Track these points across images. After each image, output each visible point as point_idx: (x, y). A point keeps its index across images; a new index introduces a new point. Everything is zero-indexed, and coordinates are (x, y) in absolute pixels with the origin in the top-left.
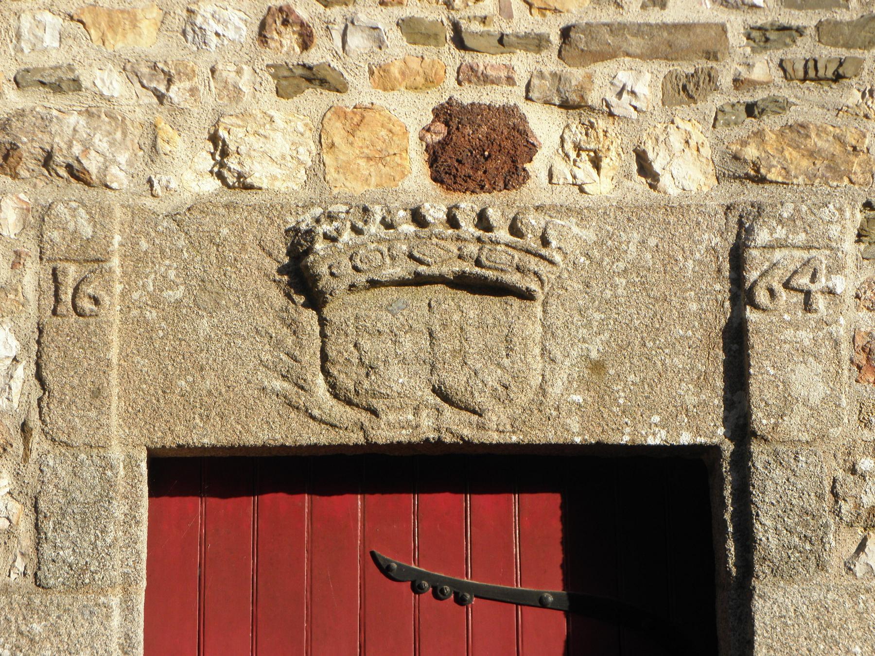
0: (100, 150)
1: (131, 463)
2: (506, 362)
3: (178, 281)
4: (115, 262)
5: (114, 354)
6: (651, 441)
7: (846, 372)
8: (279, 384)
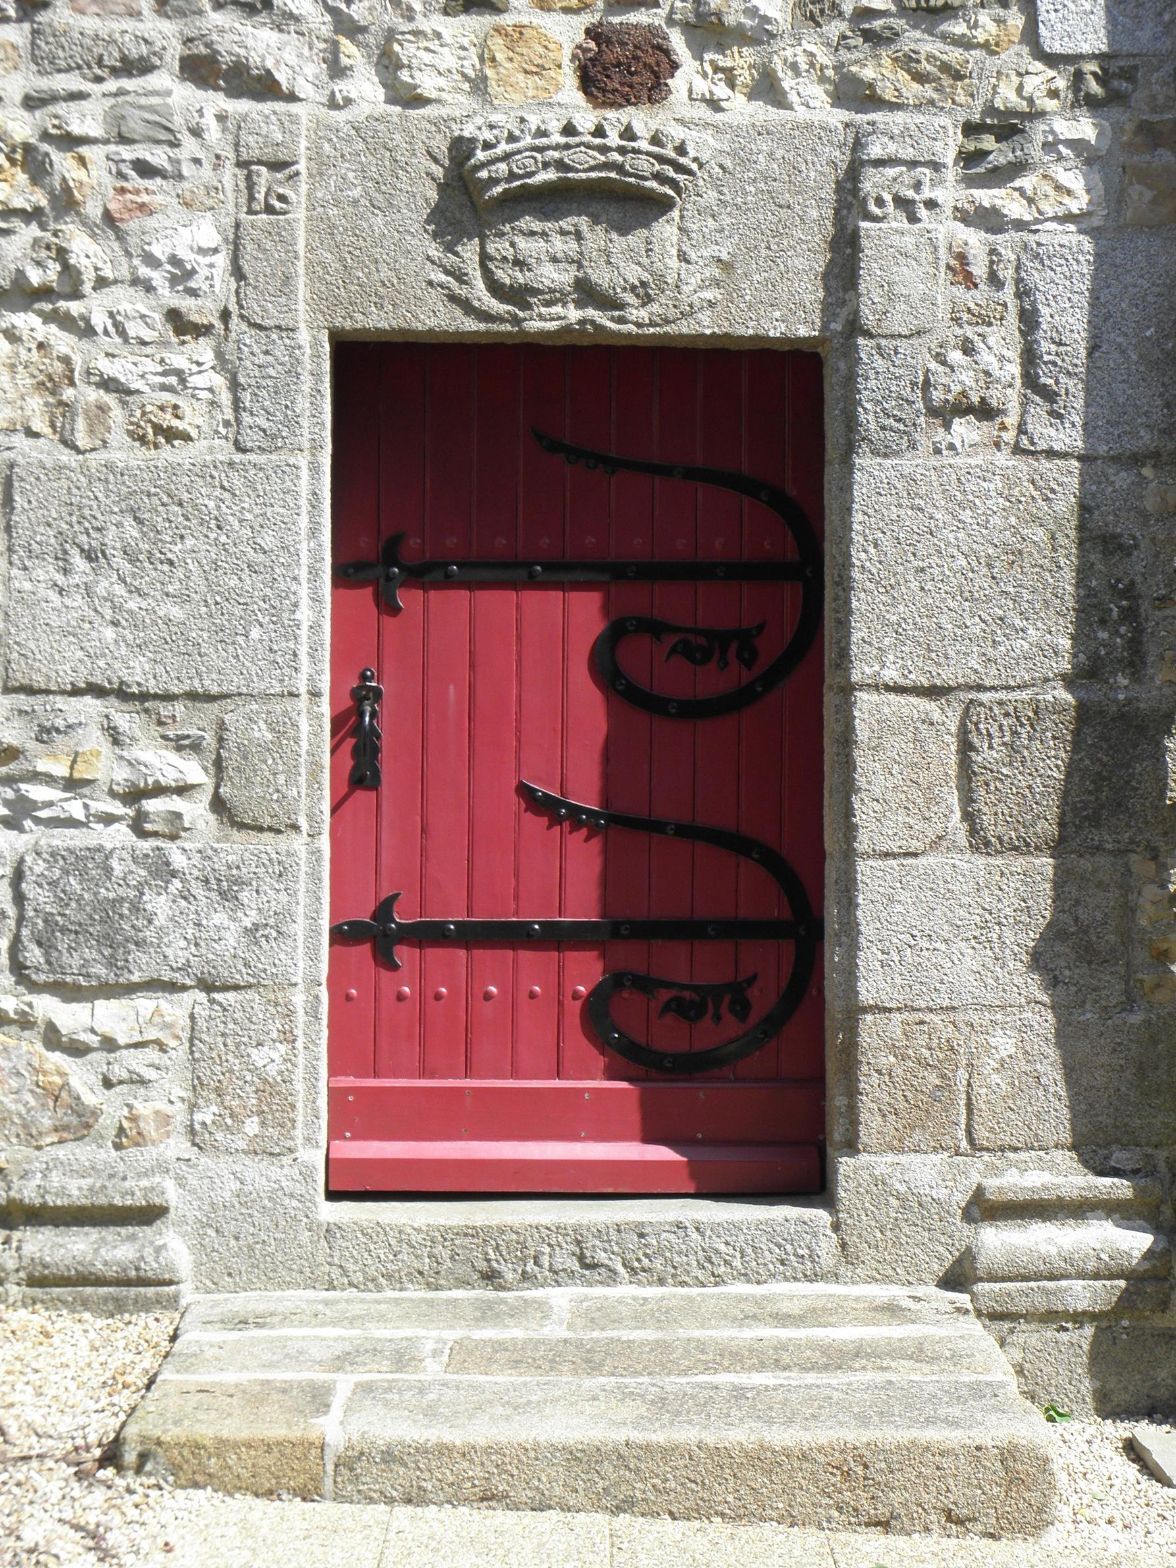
0: (289, 63)
1: (316, 343)
2: (645, 261)
3: (355, 182)
4: (302, 167)
5: (301, 247)
6: (771, 334)
7: (943, 274)
8: (443, 278)
